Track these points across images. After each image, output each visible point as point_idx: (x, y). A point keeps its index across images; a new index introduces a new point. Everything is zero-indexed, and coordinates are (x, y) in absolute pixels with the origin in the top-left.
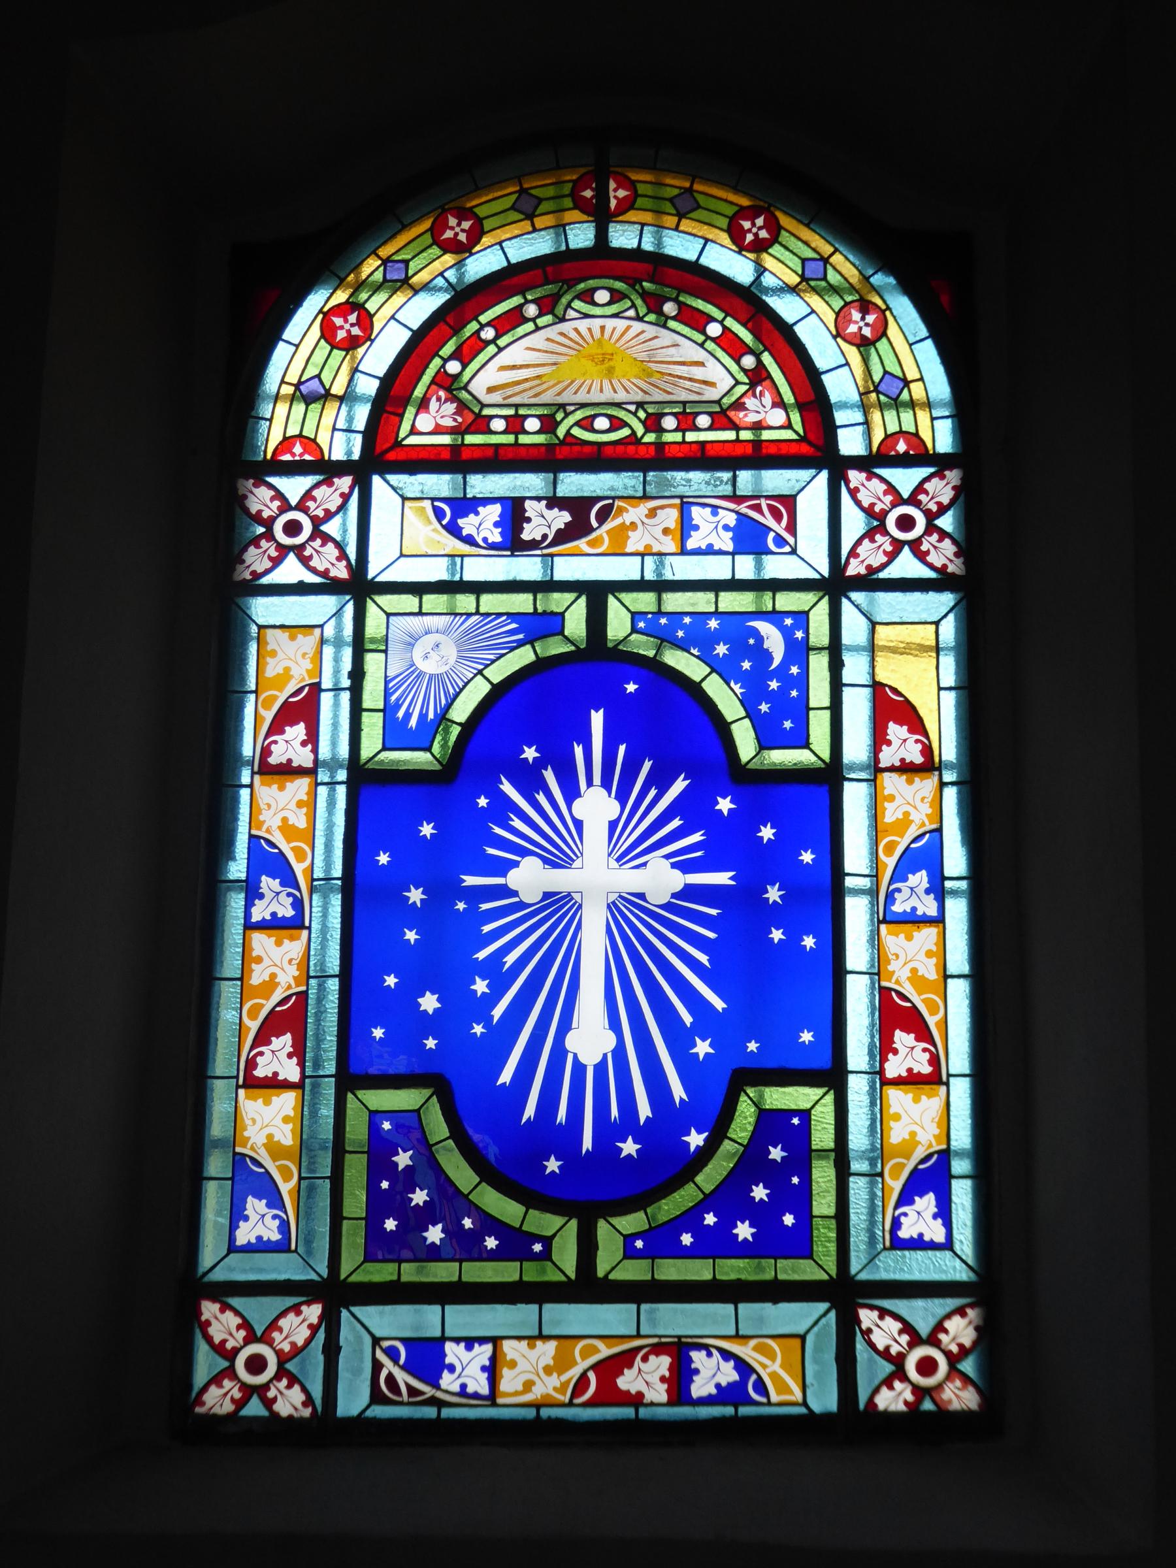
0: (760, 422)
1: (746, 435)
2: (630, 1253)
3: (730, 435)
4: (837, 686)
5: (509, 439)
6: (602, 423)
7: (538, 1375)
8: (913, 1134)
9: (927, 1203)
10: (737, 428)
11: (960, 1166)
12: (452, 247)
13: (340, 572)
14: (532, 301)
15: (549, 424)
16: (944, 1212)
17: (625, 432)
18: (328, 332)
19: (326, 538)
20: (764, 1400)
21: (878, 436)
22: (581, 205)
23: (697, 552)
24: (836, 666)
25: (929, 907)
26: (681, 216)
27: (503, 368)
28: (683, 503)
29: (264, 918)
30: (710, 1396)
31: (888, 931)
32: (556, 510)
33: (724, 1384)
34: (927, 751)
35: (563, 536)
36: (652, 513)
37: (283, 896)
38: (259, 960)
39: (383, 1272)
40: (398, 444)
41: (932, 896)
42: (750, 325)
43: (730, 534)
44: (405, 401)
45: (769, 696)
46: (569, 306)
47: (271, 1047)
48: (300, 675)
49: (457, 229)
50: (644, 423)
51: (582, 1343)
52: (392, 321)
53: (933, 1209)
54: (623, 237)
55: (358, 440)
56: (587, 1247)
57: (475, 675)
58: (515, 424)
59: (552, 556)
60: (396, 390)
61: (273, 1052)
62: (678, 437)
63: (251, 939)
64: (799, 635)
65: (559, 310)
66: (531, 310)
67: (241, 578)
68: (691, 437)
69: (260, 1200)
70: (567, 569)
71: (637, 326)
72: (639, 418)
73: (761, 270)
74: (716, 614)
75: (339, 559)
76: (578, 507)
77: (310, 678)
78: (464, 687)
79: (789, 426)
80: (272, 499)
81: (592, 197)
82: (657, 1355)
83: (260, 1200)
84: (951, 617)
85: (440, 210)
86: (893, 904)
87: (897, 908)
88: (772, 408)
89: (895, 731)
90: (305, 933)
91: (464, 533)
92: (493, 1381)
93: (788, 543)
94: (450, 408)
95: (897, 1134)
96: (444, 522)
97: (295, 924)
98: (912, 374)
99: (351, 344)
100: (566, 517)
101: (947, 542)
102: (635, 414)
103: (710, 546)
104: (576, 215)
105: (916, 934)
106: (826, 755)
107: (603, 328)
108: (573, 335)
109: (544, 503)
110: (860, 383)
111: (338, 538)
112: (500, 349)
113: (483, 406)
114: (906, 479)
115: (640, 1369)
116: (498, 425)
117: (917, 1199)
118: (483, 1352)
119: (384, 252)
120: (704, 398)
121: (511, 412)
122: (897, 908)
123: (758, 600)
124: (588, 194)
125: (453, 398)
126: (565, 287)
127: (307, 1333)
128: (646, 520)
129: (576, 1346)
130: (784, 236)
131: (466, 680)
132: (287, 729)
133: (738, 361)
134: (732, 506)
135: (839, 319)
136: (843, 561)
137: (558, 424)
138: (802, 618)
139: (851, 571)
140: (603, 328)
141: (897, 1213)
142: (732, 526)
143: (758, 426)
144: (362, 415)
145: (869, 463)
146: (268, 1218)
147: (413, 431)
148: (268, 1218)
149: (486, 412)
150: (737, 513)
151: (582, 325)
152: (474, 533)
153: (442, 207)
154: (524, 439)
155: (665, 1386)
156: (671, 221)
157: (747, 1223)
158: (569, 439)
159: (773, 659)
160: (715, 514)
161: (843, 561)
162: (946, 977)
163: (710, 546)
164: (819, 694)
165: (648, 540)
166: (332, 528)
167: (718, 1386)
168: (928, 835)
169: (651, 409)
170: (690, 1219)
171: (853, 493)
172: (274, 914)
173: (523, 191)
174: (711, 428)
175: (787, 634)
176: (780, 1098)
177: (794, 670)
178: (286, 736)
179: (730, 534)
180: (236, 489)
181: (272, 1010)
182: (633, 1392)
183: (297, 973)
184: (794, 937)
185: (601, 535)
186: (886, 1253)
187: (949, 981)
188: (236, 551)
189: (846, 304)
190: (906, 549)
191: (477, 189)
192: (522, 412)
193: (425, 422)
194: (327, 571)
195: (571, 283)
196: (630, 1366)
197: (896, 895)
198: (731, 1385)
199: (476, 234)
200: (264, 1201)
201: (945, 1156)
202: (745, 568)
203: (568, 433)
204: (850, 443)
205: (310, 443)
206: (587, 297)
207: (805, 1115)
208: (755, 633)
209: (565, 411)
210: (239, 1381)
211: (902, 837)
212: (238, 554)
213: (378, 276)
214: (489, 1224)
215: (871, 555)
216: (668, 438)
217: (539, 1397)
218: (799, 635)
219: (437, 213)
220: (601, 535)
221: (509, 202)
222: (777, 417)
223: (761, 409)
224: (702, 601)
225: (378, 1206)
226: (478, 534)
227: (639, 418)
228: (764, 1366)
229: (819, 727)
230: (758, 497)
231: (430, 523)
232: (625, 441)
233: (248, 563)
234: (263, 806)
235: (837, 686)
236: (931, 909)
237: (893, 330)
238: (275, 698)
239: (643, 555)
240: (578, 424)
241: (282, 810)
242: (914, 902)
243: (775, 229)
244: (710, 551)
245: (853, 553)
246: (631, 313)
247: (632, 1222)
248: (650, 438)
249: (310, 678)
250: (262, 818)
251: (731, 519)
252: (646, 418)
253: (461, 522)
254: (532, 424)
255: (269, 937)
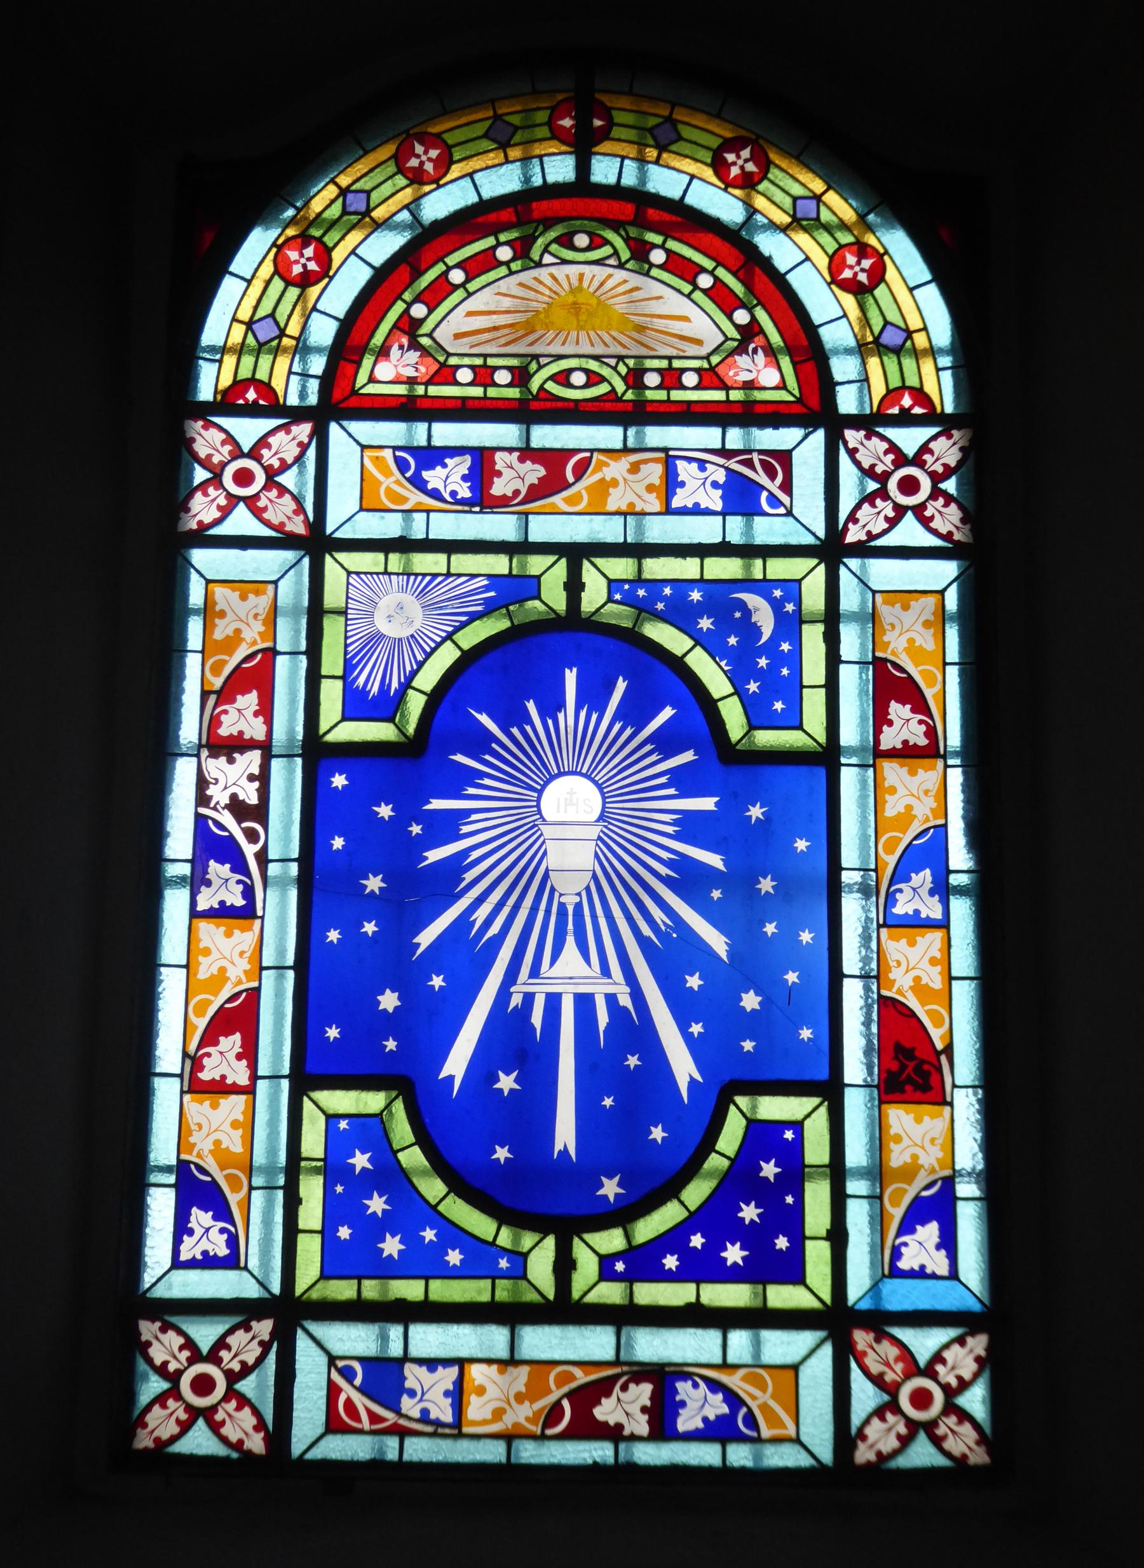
0: (752, 381)
1: (736, 395)
2: (606, 1272)
3: (718, 395)
4: (833, 660)
5: (477, 392)
6: (578, 378)
7: (509, 1404)
8: (915, 1157)
9: (930, 1232)
10: (727, 388)
11: (966, 1189)
12: (417, 178)
13: (297, 527)
14: (507, 243)
15: (521, 377)
16: (948, 1242)
17: (603, 389)
18: (281, 270)
19: (283, 490)
20: (755, 1434)
21: (878, 390)
22: (557, 135)
23: (683, 511)
24: (832, 640)
25: (932, 909)
26: (662, 148)
27: (470, 314)
28: (668, 456)
29: (194, 1257)
30: (697, 1430)
31: (889, 934)
32: (528, 463)
33: (712, 1417)
34: (931, 733)
35: (537, 492)
36: (635, 468)
37: (232, 884)
38: (207, 952)
39: (343, 1290)
40: (355, 393)
41: (937, 897)
42: (741, 273)
43: (720, 492)
44: (362, 350)
45: (759, 675)
46: (546, 250)
47: (219, 1048)
48: (252, 637)
49: (424, 157)
50: (625, 379)
51: (560, 1369)
52: (353, 257)
53: (936, 1239)
54: (604, 171)
55: (314, 386)
56: (564, 1266)
57: (444, 640)
58: (483, 375)
59: (527, 514)
60: (355, 338)
61: (239, 710)
62: (661, 395)
63: (198, 929)
64: (790, 607)
65: (535, 254)
66: (505, 253)
67: (187, 528)
68: (677, 395)
69: (206, 1212)
70: (543, 529)
71: (621, 275)
72: (619, 373)
73: (752, 211)
74: (702, 582)
75: (296, 512)
76: (553, 459)
77: (263, 641)
78: (434, 650)
79: (783, 386)
80: (223, 443)
81: (572, 127)
82: (637, 1383)
83: (206, 1212)
84: (955, 585)
85: (404, 136)
86: (894, 906)
87: (899, 910)
88: (765, 366)
89: (898, 711)
90: (258, 922)
91: (430, 487)
92: (458, 1407)
93: (782, 504)
94: (413, 356)
95: (897, 1157)
96: (408, 475)
97: (247, 913)
98: (914, 323)
99: (306, 281)
100: (541, 471)
101: (953, 506)
102: (615, 368)
103: (697, 505)
104: (553, 147)
105: (919, 939)
106: (822, 738)
107: (581, 276)
108: (548, 281)
109: (516, 454)
110: (856, 330)
111: (295, 491)
112: (470, 294)
113: (449, 355)
114: (910, 439)
115: (619, 1399)
116: (465, 375)
117: (919, 1227)
118: (447, 1377)
119: (344, 181)
120: (686, 354)
121: (479, 361)
122: (899, 910)
123: (748, 568)
124: (567, 123)
125: (414, 345)
126: (541, 228)
127: (258, 1351)
128: (629, 477)
129: (549, 1373)
130: (774, 173)
131: (433, 645)
132: (239, 697)
133: (730, 317)
134: (721, 461)
135: (834, 263)
136: (841, 526)
137: (531, 376)
138: (793, 587)
139: (850, 538)
140: (581, 276)
141: (898, 1241)
142: (721, 482)
143: (750, 385)
144: (318, 364)
145: (869, 423)
146: (232, 883)
147: (372, 379)
148: (214, 1233)
149: (453, 361)
150: (727, 469)
151: (561, 272)
152: (440, 486)
153: (407, 132)
154: (492, 392)
155: (646, 1417)
156: (652, 153)
157: (738, 1245)
158: (542, 395)
159: (761, 634)
160: (702, 469)
161: (841, 526)
162: (951, 978)
163: (697, 505)
164: (814, 669)
165: (630, 497)
166: (287, 479)
167: (705, 1420)
168: (932, 830)
169: (631, 363)
170: (673, 1239)
171: (852, 453)
172: (222, 903)
173: (497, 117)
174: (697, 387)
175: (777, 606)
176: (773, 1108)
177: (785, 647)
178: (220, 1048)
179: (720, 492)
180: (183, 432)
181: (238, 667)
182: (612, 1423)
183: (248, 967)
184: (789, 932)
185: (580, 492)
186: (886, 1280)
187: (954, 983)
188: (181, 498)
189: (841, 247)
190: (910, 514)
191: (446, 112)
192: (491, 362)
193: (385, 371)
194: (282, 524)
195: (548, 224)
196: (608, 1394)
197: (898, 895)
198: (720, 1418)
199: (445, 163)
200: (210, 1213)
201: (949, 1183)
202: (735, 529)
203: (541, 388)
204: (847, 402)
205: (265, 388)
206: (566, 241)
207: (797, 1126)
208: (742, 605)
209: (538, 363)
210: (184, 1401)
211: (904, 833)
212: (183, 501)
213: (335, 211)
214: (454, 1234)
215: (872, 519)
216: (650, 395)
217: (510, 1427)
218: (790, 607)
219: (400, 139)
220: (580, 492)
221: (481, 129)
222: (769, 377)
223: (751, 367)
224: (688, 568)
225: (332, 1214)
226: (445, 486)
227: (619, 373)
228: (754, 1398)
229: (814, 705)
230: (750, 452)
231: (392, 474)
232: (605, 398)
233: (193, 512)
234: (193, 1127)
235: (833, 660)
236: (937, 913)
237: (891, 274)
238: (209, 1003)
239: (625, 514)
240: (554, 378)
241: (216, 1131)
242: (917, 904)
243: (765, 166)
244: (696, 510)
245: (852, 518)
246: (612, 262)
247: (612, 1241)
248: (630, 395)
249: (263, 641)
250: (192, 1140)
251: (721, 476)
252: (627, 374)
253: (425, 474)
254: (503, 377)
255: (218, 926)
